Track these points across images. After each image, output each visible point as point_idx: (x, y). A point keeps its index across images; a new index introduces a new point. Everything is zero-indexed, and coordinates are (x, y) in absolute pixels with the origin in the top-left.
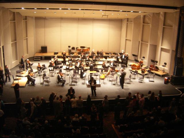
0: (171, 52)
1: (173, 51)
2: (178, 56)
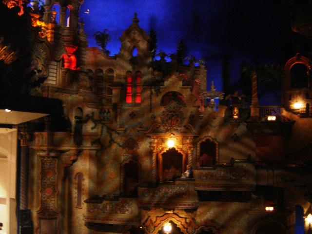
0: (8, 202)
1: (11, 199)
2: (22, 208)
